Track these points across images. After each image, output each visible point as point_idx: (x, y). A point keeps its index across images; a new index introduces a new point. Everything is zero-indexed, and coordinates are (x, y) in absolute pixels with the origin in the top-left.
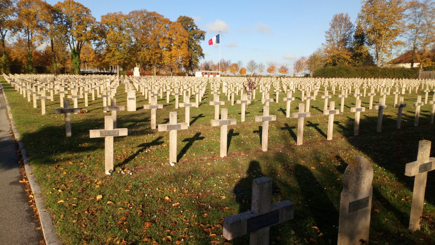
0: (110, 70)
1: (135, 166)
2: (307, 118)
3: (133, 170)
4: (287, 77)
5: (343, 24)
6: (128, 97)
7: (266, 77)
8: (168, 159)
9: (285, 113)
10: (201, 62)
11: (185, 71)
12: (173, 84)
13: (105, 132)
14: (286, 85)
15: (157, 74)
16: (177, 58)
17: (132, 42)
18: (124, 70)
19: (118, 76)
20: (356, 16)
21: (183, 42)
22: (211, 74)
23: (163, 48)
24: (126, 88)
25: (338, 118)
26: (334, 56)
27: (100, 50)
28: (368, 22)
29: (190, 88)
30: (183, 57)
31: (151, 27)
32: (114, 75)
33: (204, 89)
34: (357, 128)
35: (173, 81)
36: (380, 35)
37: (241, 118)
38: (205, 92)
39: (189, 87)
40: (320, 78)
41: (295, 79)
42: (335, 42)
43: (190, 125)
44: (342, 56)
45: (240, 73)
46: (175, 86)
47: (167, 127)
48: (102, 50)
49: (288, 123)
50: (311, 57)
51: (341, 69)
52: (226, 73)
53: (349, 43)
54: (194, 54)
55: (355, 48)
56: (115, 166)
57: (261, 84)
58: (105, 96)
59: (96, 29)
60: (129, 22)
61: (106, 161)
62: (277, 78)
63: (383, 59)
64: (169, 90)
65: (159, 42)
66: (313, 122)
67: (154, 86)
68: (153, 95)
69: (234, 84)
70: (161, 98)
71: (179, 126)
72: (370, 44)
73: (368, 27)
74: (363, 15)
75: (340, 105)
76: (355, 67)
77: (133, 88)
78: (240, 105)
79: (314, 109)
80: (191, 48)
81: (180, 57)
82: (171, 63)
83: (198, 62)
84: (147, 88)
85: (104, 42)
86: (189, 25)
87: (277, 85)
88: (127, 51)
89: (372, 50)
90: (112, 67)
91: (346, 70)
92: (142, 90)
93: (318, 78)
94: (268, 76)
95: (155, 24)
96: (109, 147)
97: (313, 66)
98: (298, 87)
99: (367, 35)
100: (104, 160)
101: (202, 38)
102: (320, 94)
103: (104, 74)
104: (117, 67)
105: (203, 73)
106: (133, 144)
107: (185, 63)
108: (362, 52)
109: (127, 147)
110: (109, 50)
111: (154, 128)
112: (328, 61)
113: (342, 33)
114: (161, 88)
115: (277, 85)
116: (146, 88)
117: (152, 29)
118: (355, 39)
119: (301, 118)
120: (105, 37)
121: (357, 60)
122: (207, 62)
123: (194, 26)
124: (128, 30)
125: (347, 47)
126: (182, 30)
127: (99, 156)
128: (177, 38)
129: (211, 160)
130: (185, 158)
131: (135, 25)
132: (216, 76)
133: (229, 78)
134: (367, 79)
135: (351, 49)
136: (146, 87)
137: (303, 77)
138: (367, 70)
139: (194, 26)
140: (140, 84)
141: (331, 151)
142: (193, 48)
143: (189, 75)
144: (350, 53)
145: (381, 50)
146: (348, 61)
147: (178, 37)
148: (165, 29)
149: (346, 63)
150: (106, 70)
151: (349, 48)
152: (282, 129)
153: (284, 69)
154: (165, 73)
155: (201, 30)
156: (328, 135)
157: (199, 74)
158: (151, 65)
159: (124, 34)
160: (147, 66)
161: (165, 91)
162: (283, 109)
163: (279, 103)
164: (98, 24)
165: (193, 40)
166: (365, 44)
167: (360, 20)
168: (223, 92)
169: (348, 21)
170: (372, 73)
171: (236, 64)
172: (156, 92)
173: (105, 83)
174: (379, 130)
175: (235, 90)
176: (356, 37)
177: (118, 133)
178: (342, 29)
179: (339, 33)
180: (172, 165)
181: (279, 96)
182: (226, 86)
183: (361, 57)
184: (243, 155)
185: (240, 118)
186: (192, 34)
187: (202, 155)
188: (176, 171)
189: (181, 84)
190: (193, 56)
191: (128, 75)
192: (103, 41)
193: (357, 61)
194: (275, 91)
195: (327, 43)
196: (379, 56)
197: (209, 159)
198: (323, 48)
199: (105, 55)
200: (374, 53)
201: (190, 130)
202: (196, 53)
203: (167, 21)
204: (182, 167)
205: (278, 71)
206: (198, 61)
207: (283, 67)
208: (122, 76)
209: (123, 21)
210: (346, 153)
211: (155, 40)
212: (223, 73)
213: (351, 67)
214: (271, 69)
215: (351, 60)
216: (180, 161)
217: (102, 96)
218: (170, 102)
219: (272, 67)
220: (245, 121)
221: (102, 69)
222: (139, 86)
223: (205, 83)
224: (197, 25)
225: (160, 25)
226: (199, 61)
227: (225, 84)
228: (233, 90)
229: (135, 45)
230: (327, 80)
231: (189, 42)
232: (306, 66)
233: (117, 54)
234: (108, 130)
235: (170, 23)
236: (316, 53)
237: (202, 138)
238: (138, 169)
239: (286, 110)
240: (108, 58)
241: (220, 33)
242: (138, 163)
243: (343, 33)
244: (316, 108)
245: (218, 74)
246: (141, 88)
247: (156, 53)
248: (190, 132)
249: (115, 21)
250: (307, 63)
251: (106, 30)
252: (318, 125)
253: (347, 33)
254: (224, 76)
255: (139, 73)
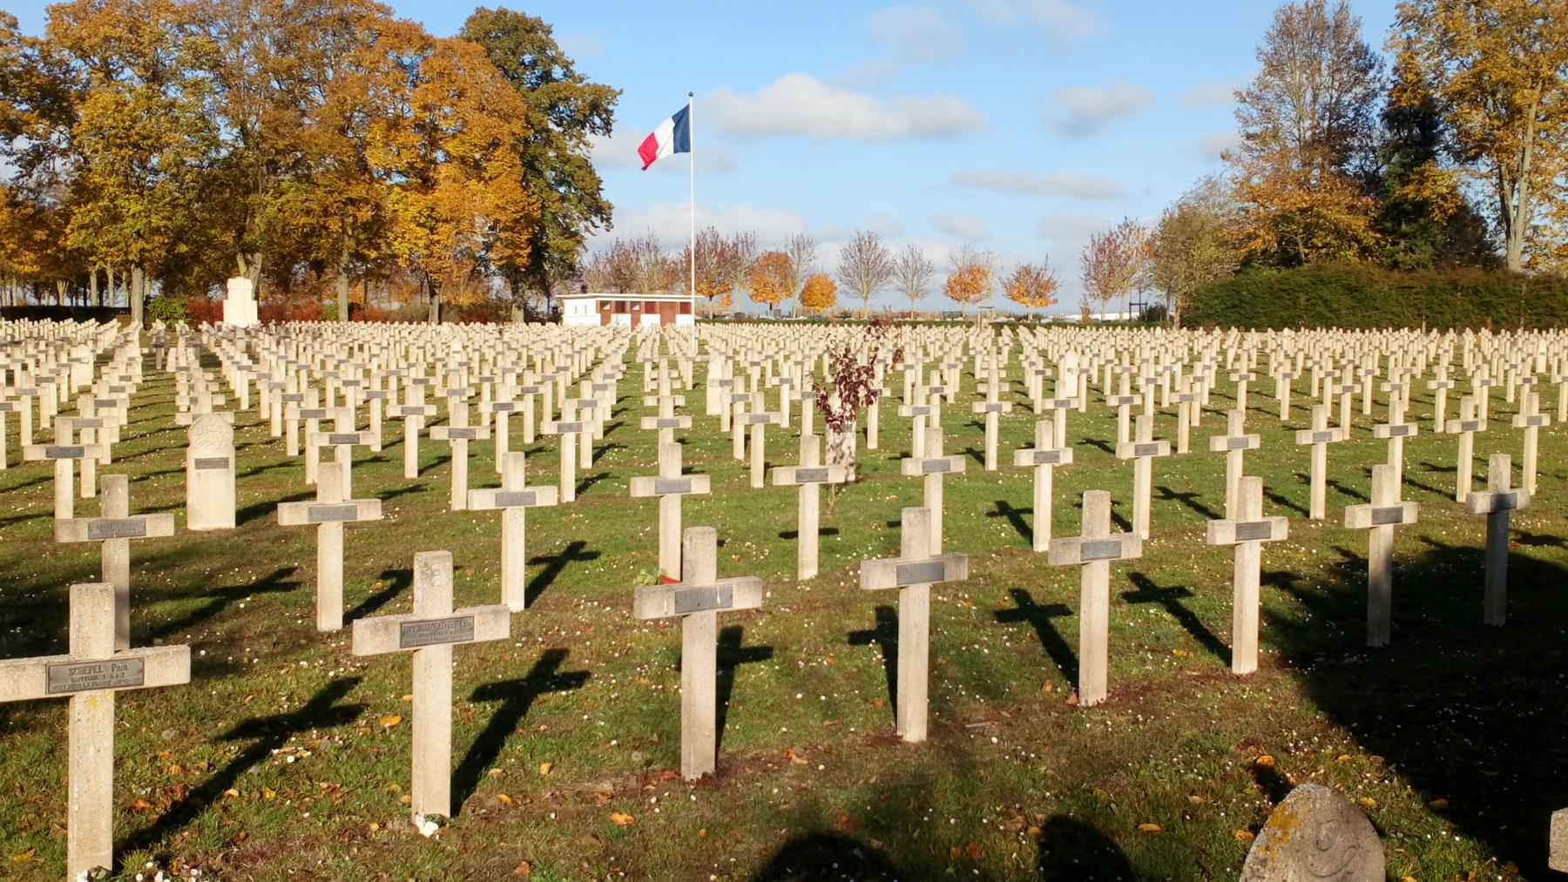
0: (93, 290)
1: (227, 845)
2: (1129, 563)
3: (217, 862)
4: (1048, 326)
5: (1327, 57)
6: (193, 454)
7: (938, 324)
8: (405, 799)
9: (1027, 532)
10: (596, 244)
11: (508, 295)
12: (440, 372)
13: (72, 672)
14: (1038, 372)
15: (356, 312)
16: (465, 225)
17: (216, 144)
18: (168, 289)
19: (136, 325)
20: (1391, 15)
21: (495, 144)
22: (650, 308)
23: (388, 174)
24: (182, 402)
25: (1297, 551)
26: (1286, 218)
27: (39, 184)
28: (1449, 43)
29: (530, 397)
30: (497, 221)
31: (320, 67)
32: (114, 322)
33: (608, 400)
34: (1378, 612)
35: (439, 355)
36: (1514, 113)
37: (796, 561)
38: (614, 414)
39: (525, 391)
40: (1217, 331)
41: (1087, 336)
42: (1291, 145)
43: (529, 601)
44: (1324, 217)
45: (804, 301)
46: (454, 384)
47: (402, 634)
48: (50, 184)
49: (1024, 585)
50: (1167, 225)
51: (1321, 281)
52: (729, 302)
53: (1361, 148)
54: (555, 207)
55: (1389, 174)
56: (122, 849)
57: (911, 367)
58: (65, 452)
59: (17, 75)
60: (200, 40)
61: (73, 825)
62: (998, 327)
63: (1535, 228)
64: (417, 411)
65: (365, 144)
66: (1161, 578)
67: (338, 384)
68: (331, 440)
69: (769, 365)
70: (376, 448)
71: (465, 624)
72: (1466, 154)
73: (1452, 68)
74: (1421, 9)
75: (1307, 480)
76: (1396, 274)
77: (221, 400)
78: (790, 496)
79: (1178, 505)
80: (540, 174)
81: (479, 221)
82: (431, 256)
83: (580, 249)
84: (299, 398)
85: (64, 145)
86: (527, 58)
87: (991, 369)
88: (192, 194)
89: (1478, 184)
90: (102, 277)
91: (1351, 290)
92: (271, 407)
93: (1209, 331)
94: (949, 320)
95: (346, 49)
96: (91, 751)
97: (1180, 266)
98: (1101, 379)
99: (1446, 108)
100: (64, 811)
101: (597, 120)
102: (1212, 420)
103: (58, 314)
104: (129, 283)
105: (603, 304)
106: (216, 717)
107: (509, 252)
108: (1426, 193)
109: (184, 734)
110: (83, 191)
111: (329, 618)
112: (1258, 245)
113: (1321, 100)
114: (377, 395)
115: (991, 369)
116: (292, 398)
117: (330, 74)
118: (1390, 129)
119: (1095, 563)
120: (71, 120)
121: (1404, 235)
122: (627, 246)
123: (554, 60)
124: (197, 85)
125: (1351, 167)
126: (487, 79)
127: (34, 794)
128: (465, 123)
129: (632, 794)
130: (491, 790)
131: (233, 54)
132: (673, 321)
133: (747, 328)
134: (1460, 333)
135: (1371, 183)
136: (292, 390)
137: (1130, 325)
138: (1455, 286)
139: (554, 60)
140: (261, 376)
141: (1249, 733)
142: (550, 175)
143: (530, 317)
144: (1368, 200)
145: (1522, 185)
146: (1359, 242)
147: (469, 117)
148: (398, 74)
149: (1351, 254)
150: (72, 293)
151: (1360, 177)
152: (1004, 616)
153: (1033, 284)
154: (395, 306)
155: (591, 82)
156: (1235, 647)
157: (581, 311)
158: (318, 266)
159: (172, 105)
160: (300, 270)
161: (393, 411)
162: (1015, 504)
163: (1000, 469)
164: (29, 51)
165: (548, 131)
166: (1443, 156)
167: (1412, 33)
168: (713, 409)
169: (1350, 37)
170: (1483, 303)
171: (778, 256)
172: (346, 425)
173: (65, 373)
174: (1495, 615)
175: (773, 399)
176: (1393, 118)
177: (142, 671)
178: (1324, 77)
179: (1309, 97)
180: (428, 829)
181: (1001, 430)
182: (723, 383)
183: (1422, 221)
184: (798, 766)
185: (791, 560)
186: (546, 102)
187: (587, 768)
188: (447, 863)
189: (486, 374)
190: (549, 216)
191: (194, 319)
192: (54, 137)
193: (1403, 243)
194: (979, 407)
195: (1249, 149)
196: (1513, 213)
197: (624, 793)
198: (1227, 174)
199: (67, 216)
200: (1488, 201)
201: (529, 634)
202: (563, 199)
203: (410, 36)
204: (478, 840)
205: (1003, 291)
206: (579, 242)
207: (1027, 271)
208: (159, 325)
209: (171, 32)
210: (1321, 745)
211: (343, 131)
212: (714, 305)
213: (1377, 273)
214: (966, 283)
215: (1370, 238)
216: (466, 808)
217: (48, 453)
218: (420, 472)
219: (971, 272)
220: (821, 575)
221: (45, 285)
222: (252, 384)
223: (614, 362)
224: (569, 56)
225: (369, 56)
226: (586, 243)
227: (718, 370)
228: (759, 409)
229: (227, 163)
230: (1254, 338)
231: (526, 142)
232: (1143, 268)
233: (135, 208)
234: (84, 658)
235: (427, 43)
236: (1193, 202)
237: (579, 679)
238: (244, 857)
239: (1030, 511)
240: (82, 227)
241: (691, 101)
242: (243, 825)
243: (1325, 98)
244: (1186, 498)
245: (685, 308)
246: (265, 398)
247: (351, 201)
248: (525, 643)
249: (121, 31)
250: (1151, 250)
251: (73, 82)
252: (1182, 591)
253: (1346, 98)
254: (717, 319)
255: (253, 307)
